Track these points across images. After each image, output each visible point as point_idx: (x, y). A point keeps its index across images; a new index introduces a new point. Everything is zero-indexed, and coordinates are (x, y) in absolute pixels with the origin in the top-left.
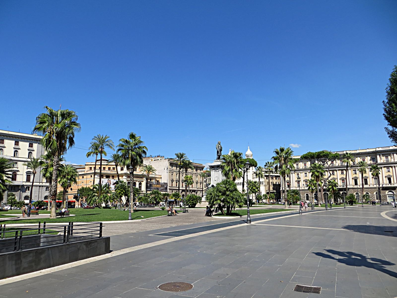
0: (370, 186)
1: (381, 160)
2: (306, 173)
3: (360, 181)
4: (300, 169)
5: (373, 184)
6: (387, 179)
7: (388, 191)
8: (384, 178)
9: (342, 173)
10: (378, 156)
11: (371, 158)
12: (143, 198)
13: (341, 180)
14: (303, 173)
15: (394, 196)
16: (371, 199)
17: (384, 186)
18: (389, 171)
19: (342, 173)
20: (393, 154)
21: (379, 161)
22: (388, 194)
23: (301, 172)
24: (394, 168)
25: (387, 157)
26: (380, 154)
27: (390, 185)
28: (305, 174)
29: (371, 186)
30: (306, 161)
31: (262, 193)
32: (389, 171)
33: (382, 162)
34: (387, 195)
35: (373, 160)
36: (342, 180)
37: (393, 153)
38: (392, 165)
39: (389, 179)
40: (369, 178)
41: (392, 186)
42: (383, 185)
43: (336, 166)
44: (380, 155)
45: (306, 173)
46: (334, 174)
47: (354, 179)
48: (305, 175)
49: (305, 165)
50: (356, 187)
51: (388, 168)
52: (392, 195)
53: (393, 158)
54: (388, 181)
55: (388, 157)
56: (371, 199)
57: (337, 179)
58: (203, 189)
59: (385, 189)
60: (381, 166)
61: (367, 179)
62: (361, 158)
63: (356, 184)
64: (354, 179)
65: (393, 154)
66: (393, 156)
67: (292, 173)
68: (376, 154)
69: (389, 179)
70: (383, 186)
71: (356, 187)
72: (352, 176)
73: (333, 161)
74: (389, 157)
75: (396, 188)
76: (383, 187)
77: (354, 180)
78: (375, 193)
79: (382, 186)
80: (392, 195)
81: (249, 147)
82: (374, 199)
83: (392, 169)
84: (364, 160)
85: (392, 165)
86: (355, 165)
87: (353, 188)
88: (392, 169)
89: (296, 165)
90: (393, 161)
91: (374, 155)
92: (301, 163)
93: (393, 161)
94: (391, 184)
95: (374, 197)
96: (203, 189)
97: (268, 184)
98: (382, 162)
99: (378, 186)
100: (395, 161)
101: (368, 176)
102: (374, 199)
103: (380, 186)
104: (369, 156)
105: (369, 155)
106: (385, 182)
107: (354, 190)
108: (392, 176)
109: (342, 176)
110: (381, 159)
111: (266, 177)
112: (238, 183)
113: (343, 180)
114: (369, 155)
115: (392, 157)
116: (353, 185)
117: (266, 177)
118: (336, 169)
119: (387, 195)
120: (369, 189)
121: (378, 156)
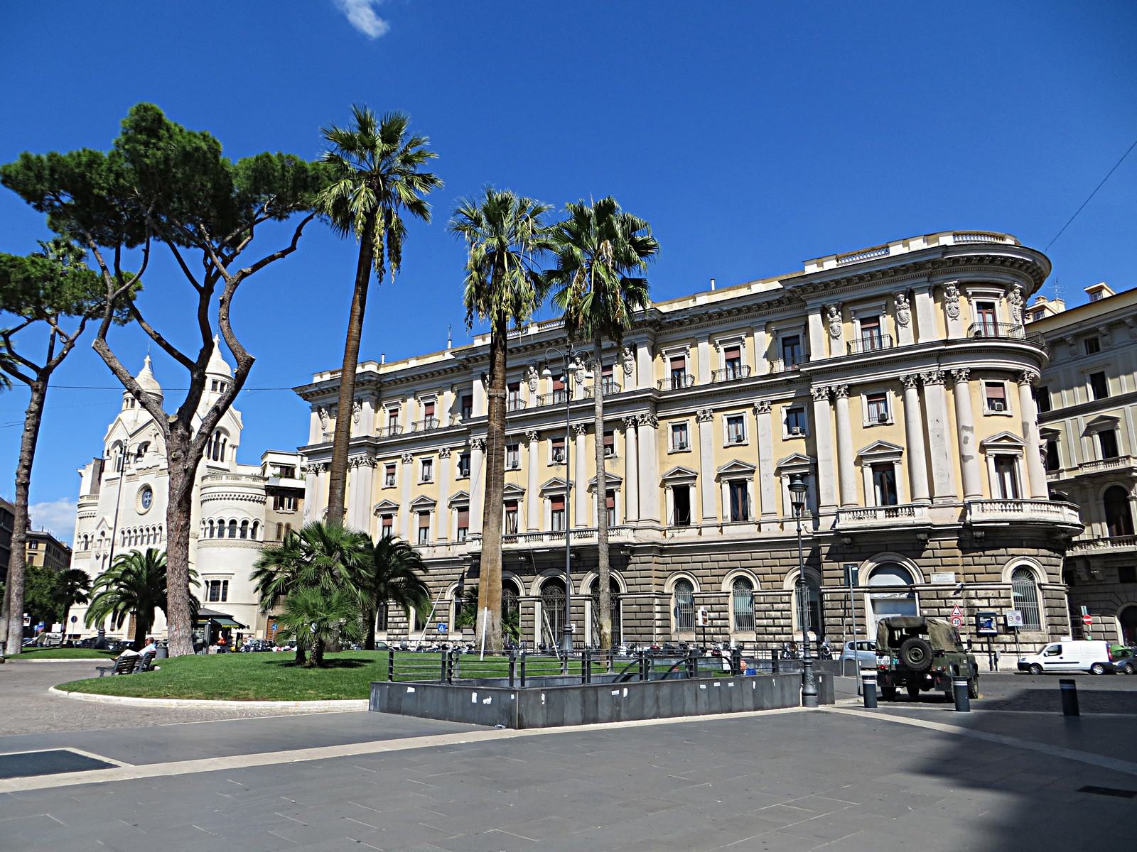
1: (831, 339)
2: (739, 419)
3: (710, 501)
6: (869, 472)
7: (869, 566)
9: (997, 404)
10: (815, 320)
11: (775, 335)
12: (692, 637)
13: (548, 502)
14: (416, 458)
15: (911, 598)
16: (765, 622)
17: (847, 522)
18: (883, 420)
22: (872, 589)
24: (912, 393)
25: (870, 322)
27: (882, 520)
28: (733, 426)
29: (711, 535)
31: (230, 587)
32: (883, 420)
33: (839, 350)
34: (867, 597)
35: (788, 355)
37: (909, 284)
38: (901, 374)
39: (884, 476)
40: (756, 475)
41: (903, 519)
42: (966, 507)
43: (755, 379)
44: (824, 312)
47: (673, 487)
50: (687, 536)
51: (876, 394)
52: (898, 596)
53: (910, 325)
54: (873, 495)
56: (765, 622)
59: (853, 546)
60: (834, 384)
61: (743, 484)
62: (716, 346)
63: (740, 513)
64: (673, 487)
65: (910, 295)
66: (913, 305)
67: (833, 399)
69: (884, 476)
70: (837, 526)
72: (662, 463)
73: (610, 368)
74: (886, 322)
75: (925, 542)
76: (968, 527)
77: (670, 493)
78: (789, 583)
79: (963, 516)
80: (898, 596)
81: (148, 359)
82: (782, 622)
83: (904, 400)
84: (733, 355)
85: (901, 374)
87: (661, 550)
88: (904, 400)
89: (388, 414)
92: (704, 346)
93: (906, 338)
94: (893, 512)
95: (786, 606)
97: (279, 536)
99: (809, 524)
101: (755, 463)
102: (782, 622)
103: (821, 529)
105: (767, 318)
106: (853, 497)
109: (998, 426)
111: (271, 499)
112: (216, 524)
114: (767, 318)
115: (905, 313)
116: (779, 517)
117: (271, 499)
119: (867, 597)
121: (815, 320)
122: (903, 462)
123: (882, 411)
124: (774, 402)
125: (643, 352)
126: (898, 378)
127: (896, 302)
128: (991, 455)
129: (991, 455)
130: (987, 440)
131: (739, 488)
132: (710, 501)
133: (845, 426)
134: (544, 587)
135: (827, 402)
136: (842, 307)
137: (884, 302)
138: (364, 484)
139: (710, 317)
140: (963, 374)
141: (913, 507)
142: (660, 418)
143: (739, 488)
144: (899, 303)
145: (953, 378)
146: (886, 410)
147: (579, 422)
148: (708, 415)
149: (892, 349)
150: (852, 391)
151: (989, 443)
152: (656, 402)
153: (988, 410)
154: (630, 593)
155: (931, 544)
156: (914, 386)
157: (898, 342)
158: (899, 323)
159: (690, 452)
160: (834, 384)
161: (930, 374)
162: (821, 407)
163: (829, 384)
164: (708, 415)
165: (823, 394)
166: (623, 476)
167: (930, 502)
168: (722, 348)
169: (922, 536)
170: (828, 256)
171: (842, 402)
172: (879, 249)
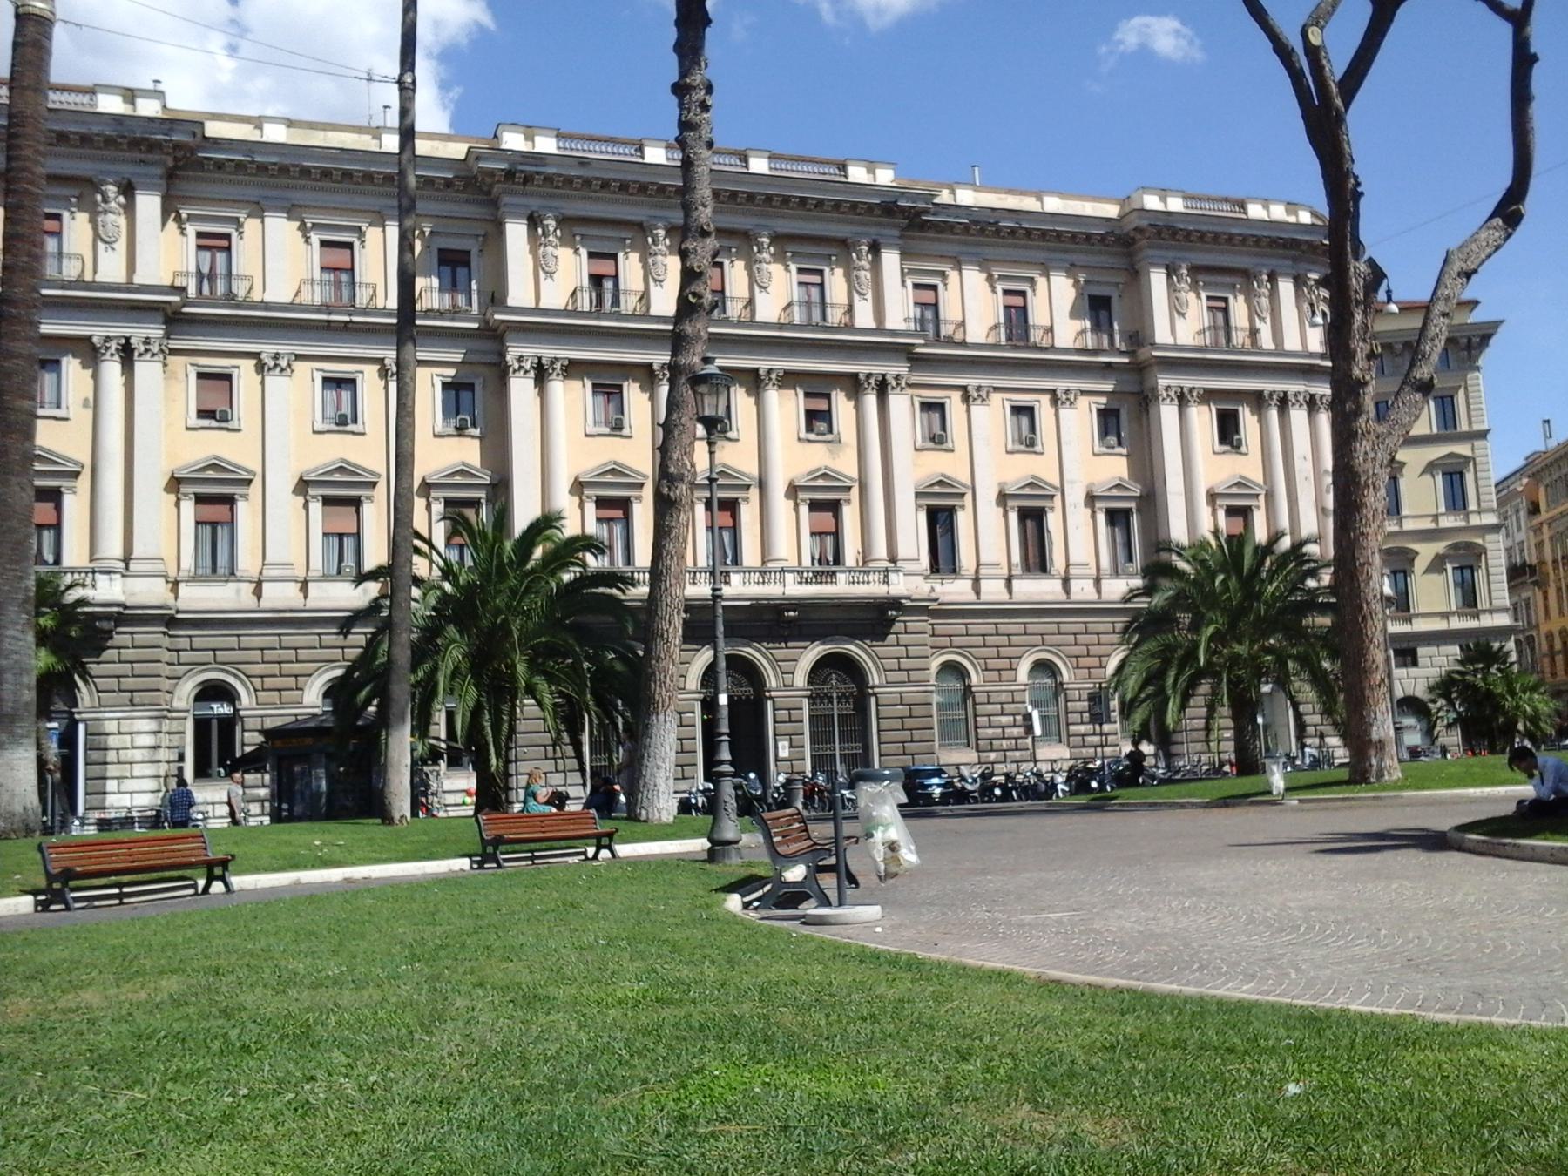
0: (267, 588)
2: (348, 383)
3: (987, 535)
4: (266, 306)
5: (300, 572)
8: (781, 507)
9: (818, 419)
10: (516, 233)
14: (996, 398)
18: (344, 421)
19: (811, 416)
20: (128, 190)
21: (519, 292)
23: (267, 348)
24: (871, 400)
26: (535, 203)
28: (331, 395)
29: (281, 596)
30: (942, 257)
35: (448, 279)
36: (815, 506)
37: (127, 170)
38: (97, 331)
40: (84, 483)
44: (534, 222)
45: (348, 383)
46: (1238, 447)
48: (188, 393)
49: (339, 258)
55: (614, 257)
57: (754, 493)
58: (1484, 611)
60: (547, 353)
61: (951, 511)
63: (1036, 559)
65: (128, 190)
66: (129, 209)
68: (494, 203)
71: (1034, 589)
75: (108, 634)
83: (95, 377)
85: (861, 368)
86: (353, 308)
90: (120, 277)
91: (1113, 258)
92: (281, 228)
93: (111, 268)
96: (1484, 611)
98: (286, 298)
100: (138, 279)
104: (1071, 270)
105: (1074, 257)
106: (784, 549)
107: (182, 637)
108: (748, 487)
110: (542, 268)
113: (824, 502)
118: (762, 363)
120: (255, 637)
121: (1158, 280)
122: (251, 497)
123: (346, 409)
124: (299, 357)
125: (149, 204)
126: (89, 338)
127: (99, 197)
128: (437, 499)
129: (437, 499)
130: (309, 472)
131: (1033, 518)
132: (987, 535)
133: (769, 437)
134: (819, 670)
135: (532, 382)
136: (1195, 270)
137: (76, 192)
138: (769, 437)
139: (998, 231)
140: (558, 366)
141: (94, 572)
142: (175, 352)
143: (1033, 518)
144: (655, 243)
145: (95, 349)
146: (944, 428)
147: (113, 332)
148: (283, 363)
149: (79, 283)
150: (573, 369)
151: (312, 477)
152: (174, 317)
153: (194, 421)
154: (889, 684)
155: (118, 639)
156: (117, 358)
157: (95, 272)
158: (852, 287)
159: (66, 419)
160: (547, 353)
161: (147, 341)
162: (521, 389)
163: (127, 332)
164: (283, 363)
165: (527, 365)
166: (86, 459)
167: (122, 565)
168: (999, 288)
169: (105, 625)
170: (544, 129)
171: (557, 386)
172: (625, 143)
